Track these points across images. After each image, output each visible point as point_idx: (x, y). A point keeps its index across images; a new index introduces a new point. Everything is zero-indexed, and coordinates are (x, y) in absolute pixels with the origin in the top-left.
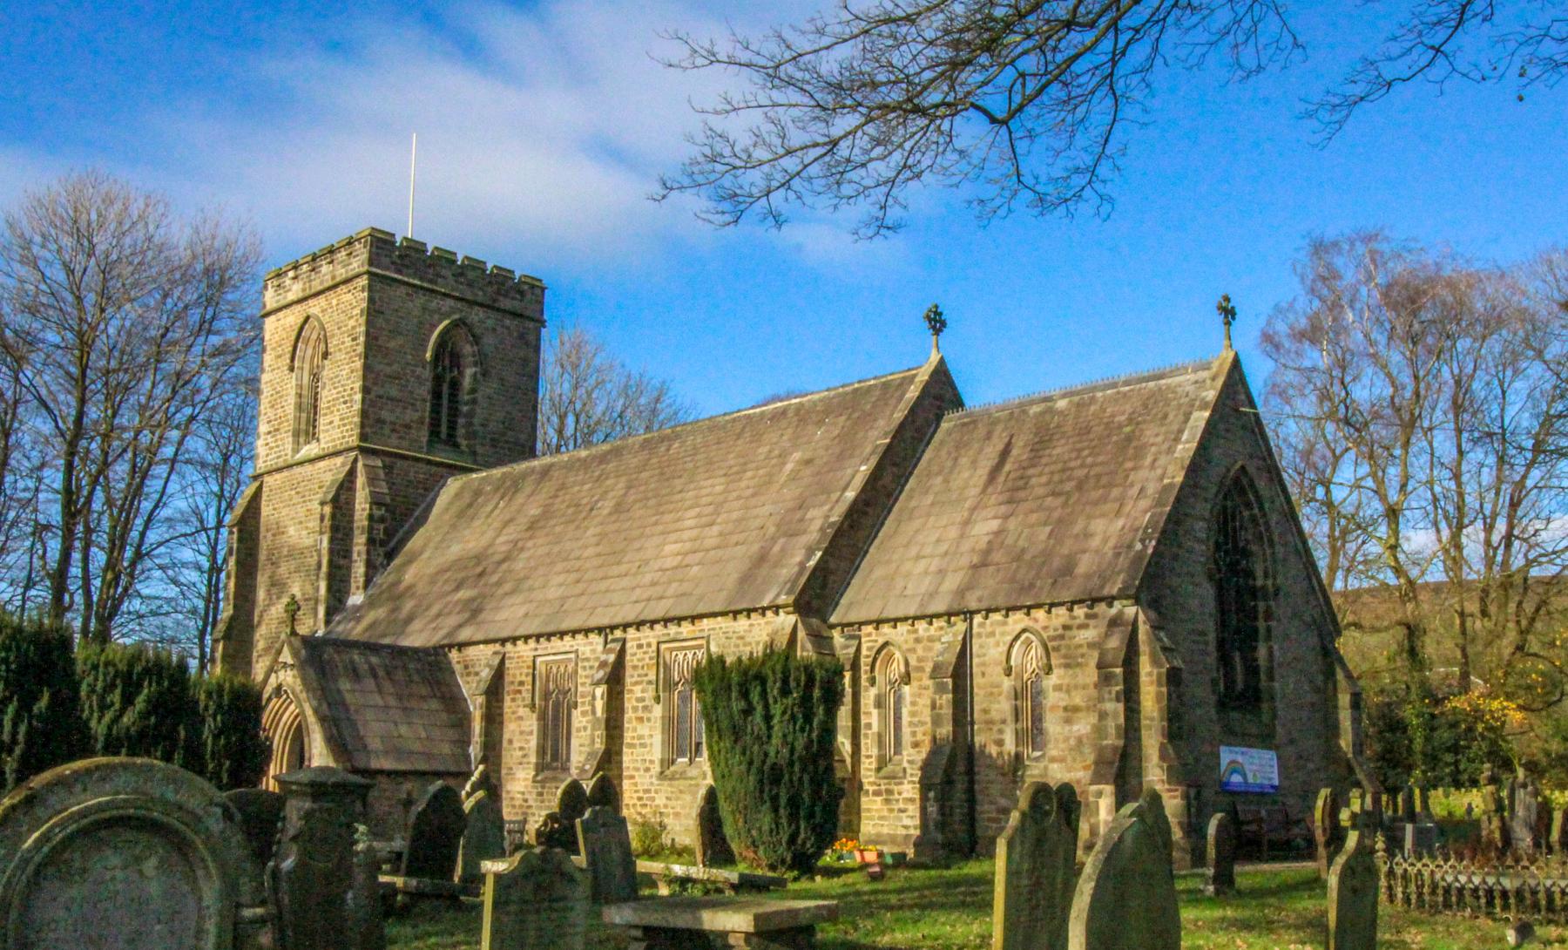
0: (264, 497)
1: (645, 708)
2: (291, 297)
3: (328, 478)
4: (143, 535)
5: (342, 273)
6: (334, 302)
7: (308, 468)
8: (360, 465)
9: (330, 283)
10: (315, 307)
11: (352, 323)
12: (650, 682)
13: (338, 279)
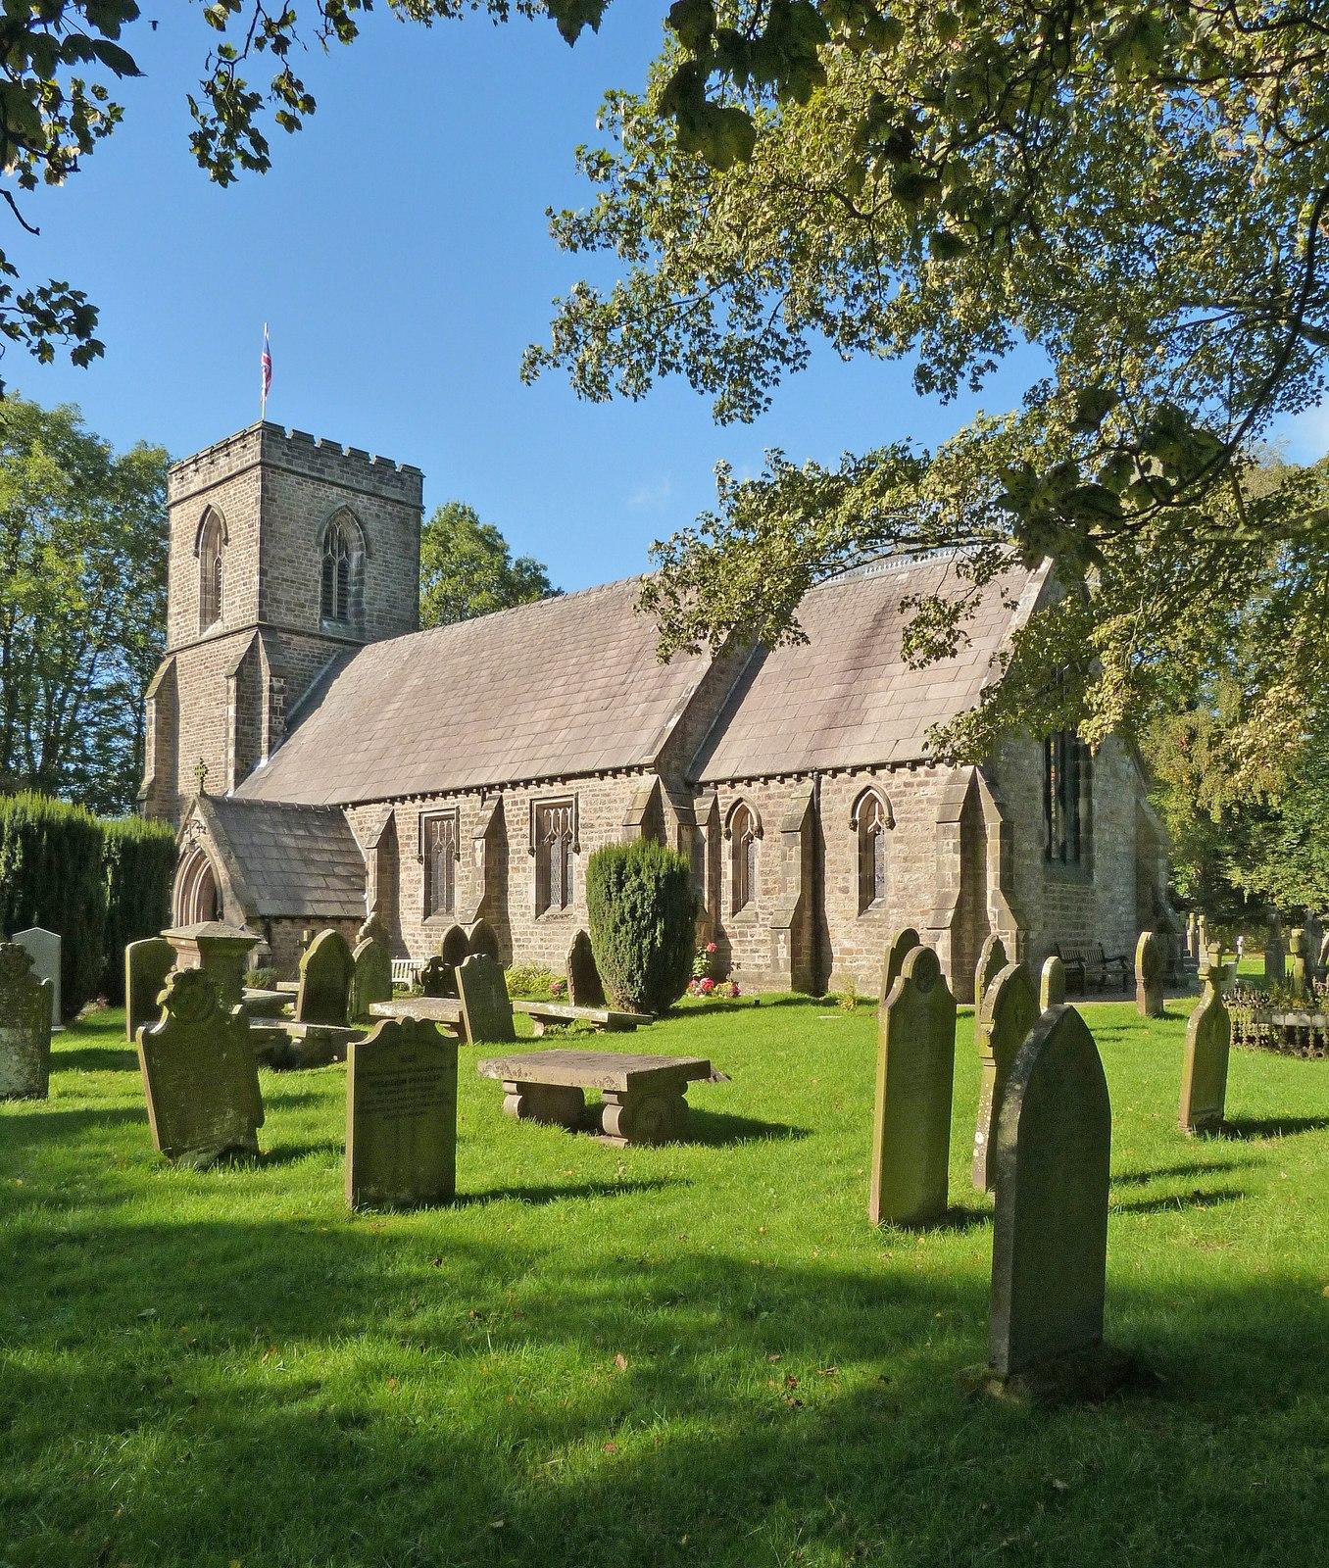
2: (194, 488)
5: (238, 465)
6: (232, 492)
7: (216, 644)
11: (248, 511)
12: (524, 836)
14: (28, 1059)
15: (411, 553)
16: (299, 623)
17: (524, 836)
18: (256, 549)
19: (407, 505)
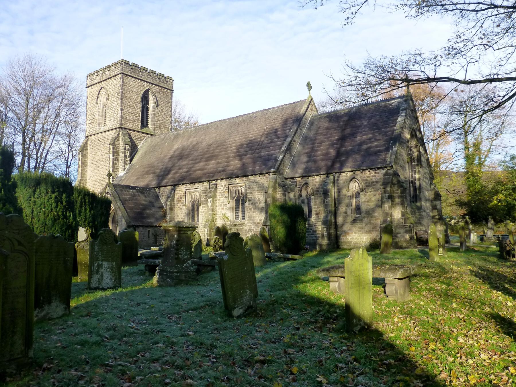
0: (89, 145)
1: (224, 205)
2: (96, 81)
3: (111, 137)
4: (46, 156)
5: (113, 74)
6: (111, 83)
7: (104, 134)
8: (121, 133)
9: (109, 77)
10: (104, 84)
11: (117, 89)
12: (226, 197)
13: (112, 76)
14: (114, 274)
15: (169, 105)
16: (134, 128)
17: (226, 197)
18: (119, 102)
19: (168, 89)
